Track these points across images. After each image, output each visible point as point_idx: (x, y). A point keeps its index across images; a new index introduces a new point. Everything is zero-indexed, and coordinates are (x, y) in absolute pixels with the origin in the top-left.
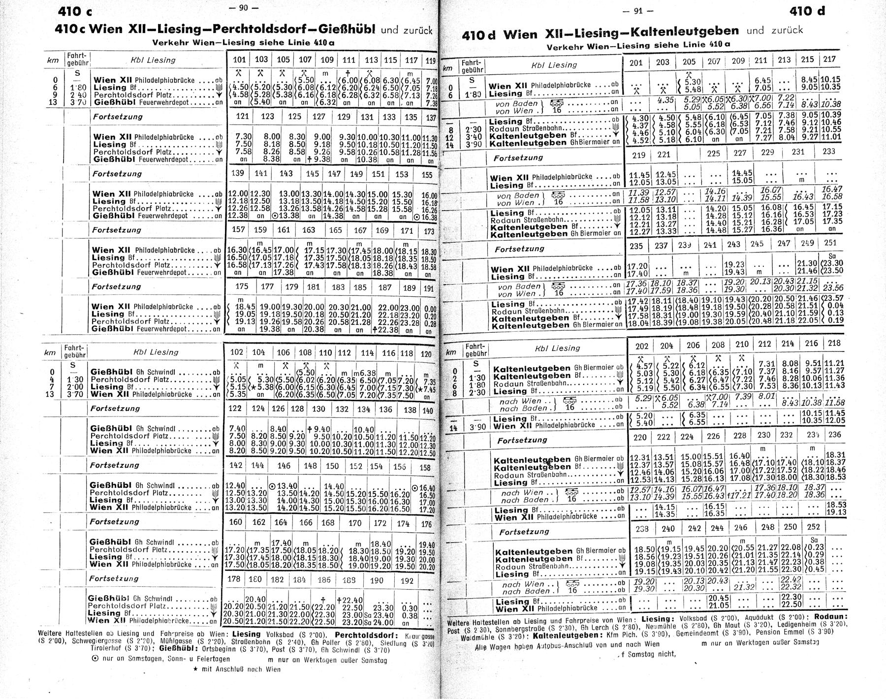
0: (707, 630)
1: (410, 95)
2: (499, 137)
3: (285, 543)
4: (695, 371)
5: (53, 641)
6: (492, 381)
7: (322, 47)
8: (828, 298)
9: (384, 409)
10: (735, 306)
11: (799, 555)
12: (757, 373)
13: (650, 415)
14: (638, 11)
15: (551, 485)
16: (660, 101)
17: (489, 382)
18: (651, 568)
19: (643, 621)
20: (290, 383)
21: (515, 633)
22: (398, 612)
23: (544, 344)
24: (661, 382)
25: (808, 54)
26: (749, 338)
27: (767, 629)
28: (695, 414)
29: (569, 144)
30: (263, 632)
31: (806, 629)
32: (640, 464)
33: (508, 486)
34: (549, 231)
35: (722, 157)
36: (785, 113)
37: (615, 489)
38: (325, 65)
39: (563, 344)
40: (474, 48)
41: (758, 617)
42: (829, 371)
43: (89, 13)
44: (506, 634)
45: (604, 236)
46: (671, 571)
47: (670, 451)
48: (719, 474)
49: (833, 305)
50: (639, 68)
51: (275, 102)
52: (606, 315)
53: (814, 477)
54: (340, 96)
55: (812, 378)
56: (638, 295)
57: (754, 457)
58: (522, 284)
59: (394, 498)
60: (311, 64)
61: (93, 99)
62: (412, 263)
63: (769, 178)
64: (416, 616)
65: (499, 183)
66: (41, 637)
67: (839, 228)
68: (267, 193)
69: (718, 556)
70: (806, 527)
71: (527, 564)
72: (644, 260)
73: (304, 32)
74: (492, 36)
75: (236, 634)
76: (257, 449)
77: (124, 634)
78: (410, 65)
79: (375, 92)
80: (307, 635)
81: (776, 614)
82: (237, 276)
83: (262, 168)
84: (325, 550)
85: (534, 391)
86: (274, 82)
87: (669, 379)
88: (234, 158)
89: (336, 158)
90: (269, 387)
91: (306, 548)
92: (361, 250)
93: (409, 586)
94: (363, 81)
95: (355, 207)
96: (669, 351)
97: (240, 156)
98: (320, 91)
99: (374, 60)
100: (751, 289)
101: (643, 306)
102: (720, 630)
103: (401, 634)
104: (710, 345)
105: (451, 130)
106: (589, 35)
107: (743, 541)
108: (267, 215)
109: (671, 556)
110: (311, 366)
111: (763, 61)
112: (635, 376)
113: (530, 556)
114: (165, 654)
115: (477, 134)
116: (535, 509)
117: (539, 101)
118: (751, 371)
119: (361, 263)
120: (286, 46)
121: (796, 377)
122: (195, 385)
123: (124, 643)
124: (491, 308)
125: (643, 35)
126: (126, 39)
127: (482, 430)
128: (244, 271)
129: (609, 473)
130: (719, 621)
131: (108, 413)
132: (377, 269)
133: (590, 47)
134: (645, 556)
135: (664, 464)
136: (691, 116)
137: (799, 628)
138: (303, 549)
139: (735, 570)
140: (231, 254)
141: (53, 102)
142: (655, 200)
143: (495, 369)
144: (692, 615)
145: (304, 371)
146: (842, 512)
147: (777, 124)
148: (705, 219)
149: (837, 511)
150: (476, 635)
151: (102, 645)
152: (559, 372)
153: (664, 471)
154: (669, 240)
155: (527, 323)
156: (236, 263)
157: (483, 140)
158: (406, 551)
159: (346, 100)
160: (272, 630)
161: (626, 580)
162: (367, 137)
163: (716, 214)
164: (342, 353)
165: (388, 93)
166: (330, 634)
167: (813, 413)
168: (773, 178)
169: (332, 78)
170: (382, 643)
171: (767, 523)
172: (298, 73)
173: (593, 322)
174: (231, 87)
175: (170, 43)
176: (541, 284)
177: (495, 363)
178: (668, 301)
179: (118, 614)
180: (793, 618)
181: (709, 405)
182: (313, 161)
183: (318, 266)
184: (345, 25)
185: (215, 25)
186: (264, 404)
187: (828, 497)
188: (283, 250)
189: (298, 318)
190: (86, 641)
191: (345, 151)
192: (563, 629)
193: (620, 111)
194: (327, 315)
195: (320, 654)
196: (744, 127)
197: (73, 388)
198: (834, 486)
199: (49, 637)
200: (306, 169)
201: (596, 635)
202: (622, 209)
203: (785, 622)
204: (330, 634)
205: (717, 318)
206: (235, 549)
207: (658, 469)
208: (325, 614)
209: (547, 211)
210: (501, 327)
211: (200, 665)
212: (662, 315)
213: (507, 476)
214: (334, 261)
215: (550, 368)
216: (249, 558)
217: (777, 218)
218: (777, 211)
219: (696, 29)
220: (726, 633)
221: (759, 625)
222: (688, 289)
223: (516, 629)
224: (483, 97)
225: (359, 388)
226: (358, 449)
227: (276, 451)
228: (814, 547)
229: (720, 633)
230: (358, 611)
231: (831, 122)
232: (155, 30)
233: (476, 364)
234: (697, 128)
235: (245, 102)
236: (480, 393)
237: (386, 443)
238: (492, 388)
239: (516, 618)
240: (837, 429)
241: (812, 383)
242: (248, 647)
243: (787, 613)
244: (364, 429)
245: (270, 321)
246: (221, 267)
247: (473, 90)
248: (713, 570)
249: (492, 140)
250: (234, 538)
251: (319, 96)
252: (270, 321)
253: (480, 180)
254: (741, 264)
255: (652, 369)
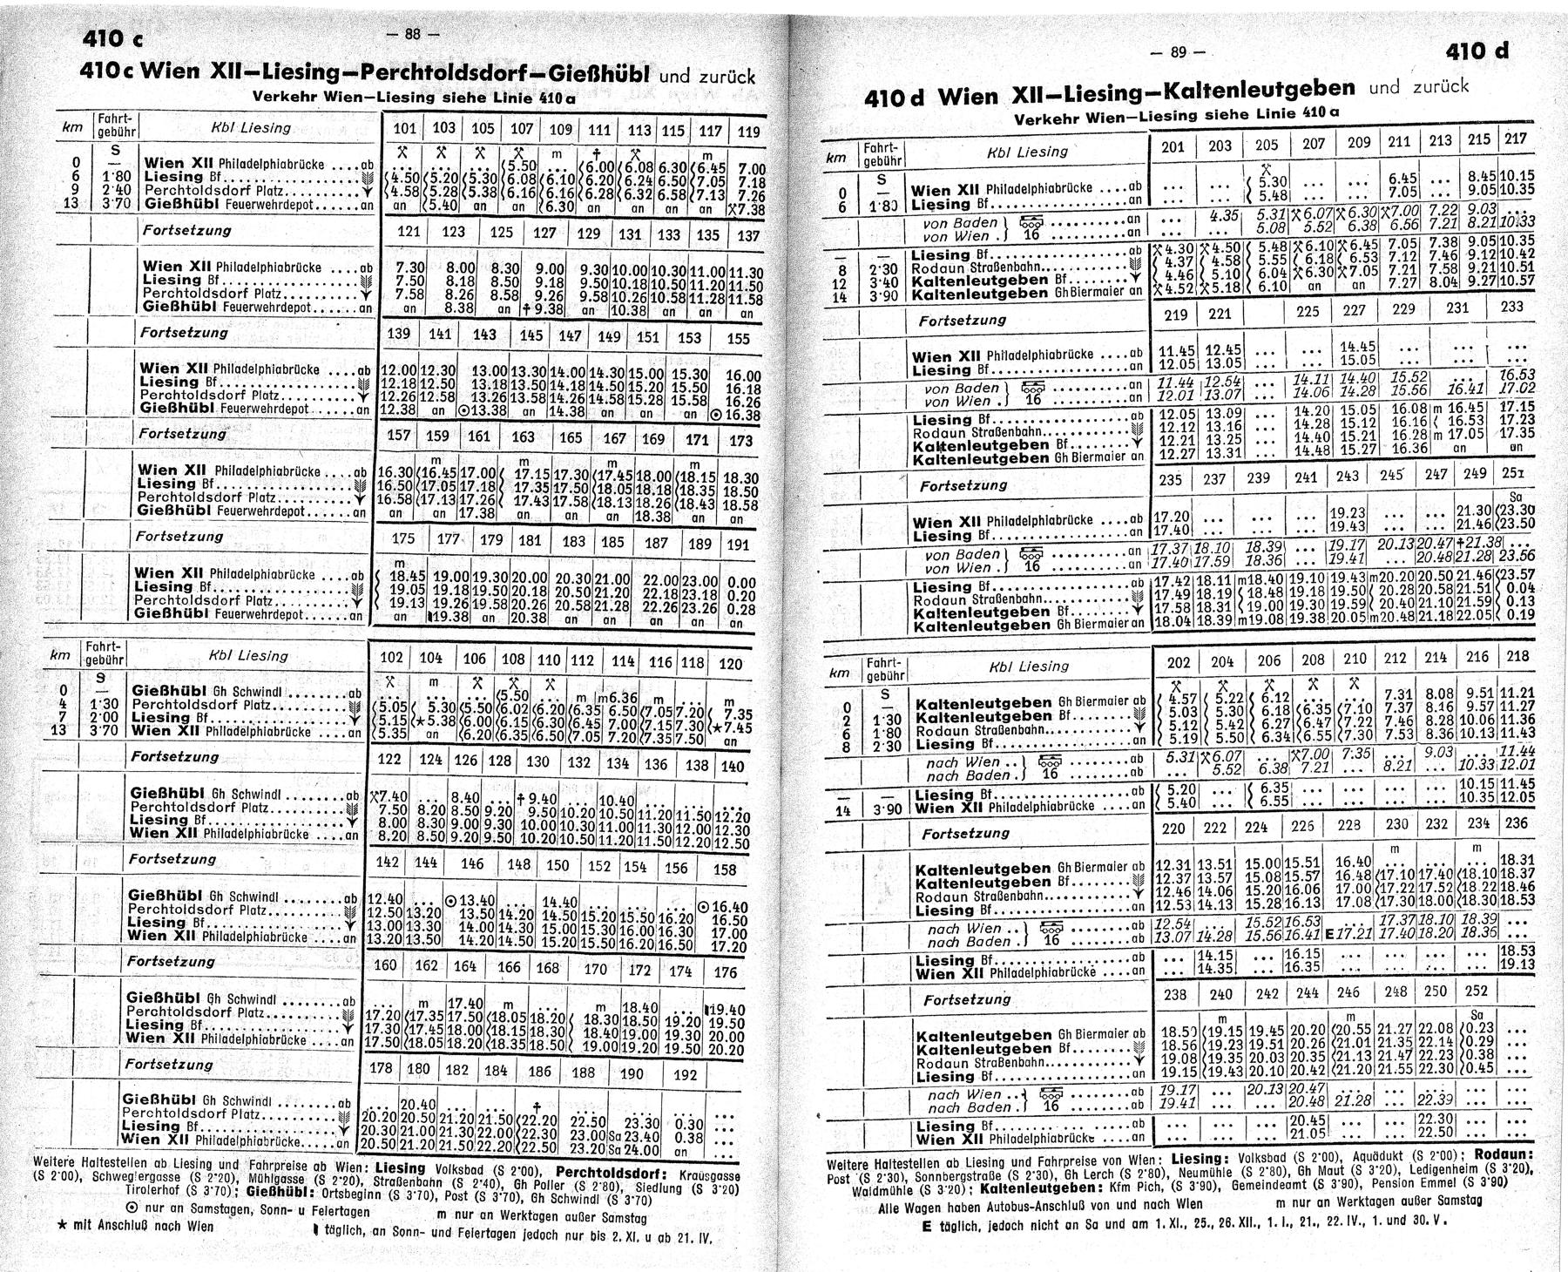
0: (1286, 1180)
1: (707, 194)
2: (929, 283)
3: (472, 1004)
4: (1272, 708)
5: (58, 1177)
6: (914, 725)
7: (554, 107)
8: (1508, 575)
9: (652, 764)
10: (1348, 589)
11: (1450, 1042)
12: (1381, 709)
13: (1190, 787)
14: (1179, 52)
15: (1015, 915)
16: (1214, 218)
17: (908, 725)
18: (1189, 1065)
19: (1174, 1162)
20: (485, 715)
21: (949, 1183)
22: (669, 1131)
23: (1006, 658)
24: (1212, 726)
25: (1479, 130)
26: (1368, 649)
27: (1391, 1178)
28: (1271, 785)
29: (1052, 296)
30: (430, 1163)
31: (1460, 1177)
32: (1174, 877)
33: (940, 917)
34: (1017, 453)
35: (1324, 319)
36: (1440, 238)
37: (1128, 922)
38: (557, 139)
39: (1039, 658)
40: (885, 120)
41: (1376, 1156)
42: (1508, 707)
43: (137, 41)
44: (934, 1185)
45: (1115, 462)
46: (1225, 1071)
47: (1226, 853)
48: (1312, 895)
49: (1517, 588)
50: (1177, 156)
51: (467, 206)
52: (1115, 607)
53: (1480, 899)
54: (583, 195)
55: (1477, 720)
56: (1173, 569)
57: (1379, 864)
58: (967, 549)
59: (665, 926)
60: (533, 137)
61: (143, 198)
62: (706, 498)
63: (1406, 356)
64: (701, 1139)
65: (928, 365)
66: (38, 1168)
67: (1528, 446)
68: (451, 370)
69: (1309, 1043)
70: (1462, 992)
71: (971, 1059)
72: (1183, 504)
73: (522, 79)
74: (918, 99)
75: (382, 1167)
76: (427, 833)
77: (186, 1164)
78: (707, 141)
79: (644, 188)
80: (508, 1171)
81: (1408, 1150)
82: (395, 519)
83: (443, 325)
84: (541, 1016)
85: (987, 743)
86: (427, 168)
87: (1226, 722)
88: (392, 305)
89: (574, 308)
90: (449, 722)
91: (509, 1013)
92: (615, 474)
93: (688, 1084)
94: (623, 169)
95: (606, 395)
96: (1226, 671)
97: (403, 302)
98: (547, 186)
99: (644, 130)
100: (1377, 558)
101: (1181, 589)
102: (1310, 1180)
103: (673, 1171)
104: (1299, 661)
105: (843, 270)
106: (1089, 96)
107: (1351, 1017)
108: (450, 410)
109: (1226, 1044)
110: (523, 684)
111: (1404, 143)
112: (1165, 716)
113: (977, 1044)
114: (255, 1203)
115: (889, 277)
116: (986, 959)
117: (1000, 218)
118: (1371, 707)
119: (615, 499)
120: (490, 104)
121: (1451, 720)
122: (316, 716)
123: (185, 1182)
124: (912, 594)
125: (1185, 97)
126: (206, 90)
127: (894, 815)
128: (407, 510)
129: (1119, 891)
130: (1308, 1162)
131: (162, 765)
132: (642, 510)
133: (1092, 118)
134: (1179, 1044)
135: (1215, 877)
136: (1269, 244)
137: (1447, 1177)
138: (503, 1015)
139: (1336, 1070)
140: (385, 479)
141: (71, 202)
142: (1205, 395)
143: (920, 704)
144: (1261, 1151)
145: (511, 694)
146: (1528, 964)
147: (1426, 258)
148: (1292, 431)
149: (1518, 964)
150: (881, 1186)
151: (145, 1183)
152: (1032, 710)
153: (1214, 890)
154: (1227, 469)
155: (975, 620)
156: (394, 496)
157: (900, 289)
158: (683, 1021)
159: (593, 202)
160: (446, 1162)
161: (1146, 1088)
162: (630, 270)
163: (1311, 421)
164: (579, 662)
165: (668, 192)
166: (548, 1169)
167: (1478, 783)
168: (1412, 356)
169: (568, 163)
170: (639, 1187)
171: (1397, 983)
172: (508, 153)
173: (1092, 619)
174: (389, 177)
175: (284, 98)
176: (1001, 549)
177: (918, 693)
178: (1225, 581)
179: (176, 1127)
180: (1437, 1157)
181: (1296, 768)
182: (532, 313)
183: (538, 502)
184: (596, 67)
185: (364, 65)
186: (441, 751)
187: (1503, 937)
188: (477, 472)
189: (500, 597)
190: (117, 1177)
191: (590, 295)
192: (1033, 1176)
193: (1144, 236)
194: (553, 593)
195: (528, 1206)
196: (1371, 264)
197: (100, 720)
198: (1514, 917)
199: (52, 1168)
200: (518, 326)
201: (1092, 1188)
202: (1146, 412)
203: (1422, 1164)
204: (548, 1169)
205: (1317, 611)
206: (383, 1014)
207: (1204, 886)
208: (540, 1133)
209: (1014, 416)
210: (931, 628)
211: (322, 1221)
212: (1215, 606)
213: (939, 898)
214: (527, 492)
215: (1016, 704)
216: (409, 1031)
217: (1420, 428)
218: (1419, 415)
219: (1279, 86)
220: (1319, 1185)
221: (1377, 1171)
222: (1265, 557)
223: (951, 1177)
224: (901, 211)
225: (607, 725)
226: (606, 834)
227: (461, 836)
228: (1477, 1027)
229: (1309, 1184)
230: (598, 1129)
231: (1517, 253)
232: (1059, 96)
233: (886, 695)
234: (1279, 267)
235: (413, 205)
236: (892, 747)
237: (655, 826)
238: (914, 738)
239: (950, 1156)
240: (1520, 814)
241: (1478, 728)
242: (403, 1191)
243: (1426, 1149)
244: (617, 800)
245: (451, 603)
246: (366, 504)
247: (881, 199)
248: (1299, 1070)
249: (917, 288)
250: (381, 995)
251: (544, 195)
252: (451, 603)
253: (890, 360)
254: (1359, 513)
255: (1196, 703)
